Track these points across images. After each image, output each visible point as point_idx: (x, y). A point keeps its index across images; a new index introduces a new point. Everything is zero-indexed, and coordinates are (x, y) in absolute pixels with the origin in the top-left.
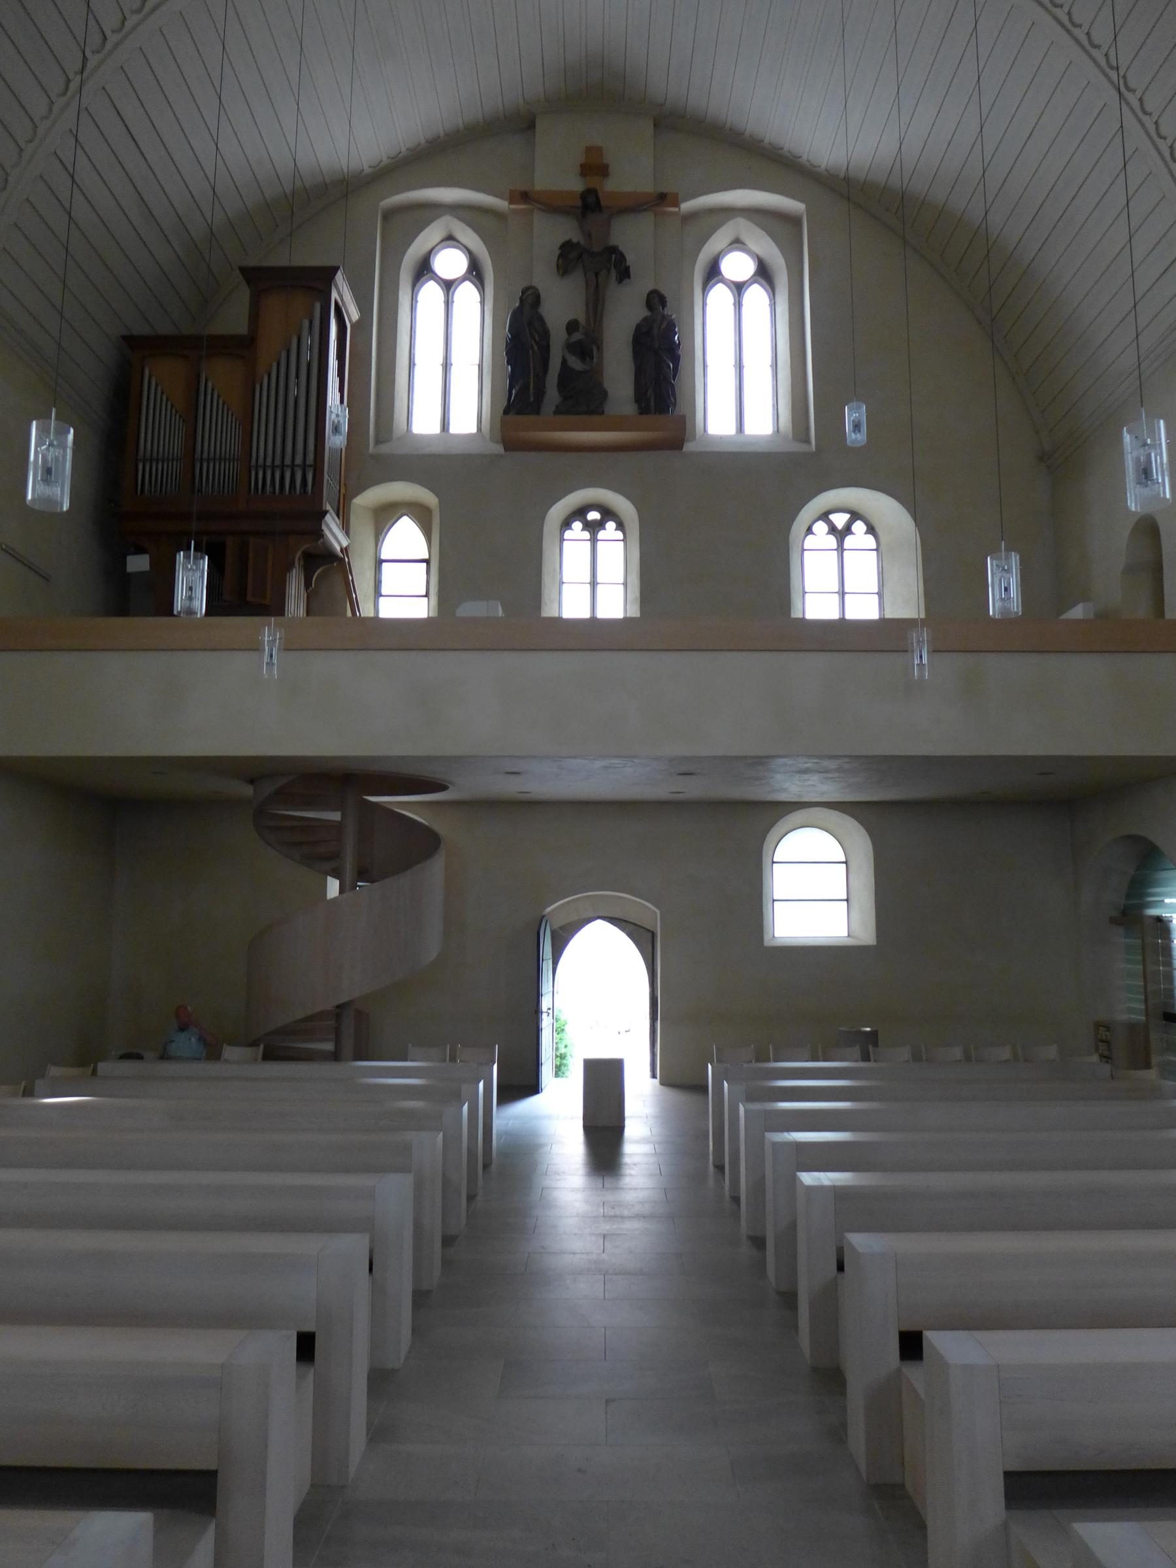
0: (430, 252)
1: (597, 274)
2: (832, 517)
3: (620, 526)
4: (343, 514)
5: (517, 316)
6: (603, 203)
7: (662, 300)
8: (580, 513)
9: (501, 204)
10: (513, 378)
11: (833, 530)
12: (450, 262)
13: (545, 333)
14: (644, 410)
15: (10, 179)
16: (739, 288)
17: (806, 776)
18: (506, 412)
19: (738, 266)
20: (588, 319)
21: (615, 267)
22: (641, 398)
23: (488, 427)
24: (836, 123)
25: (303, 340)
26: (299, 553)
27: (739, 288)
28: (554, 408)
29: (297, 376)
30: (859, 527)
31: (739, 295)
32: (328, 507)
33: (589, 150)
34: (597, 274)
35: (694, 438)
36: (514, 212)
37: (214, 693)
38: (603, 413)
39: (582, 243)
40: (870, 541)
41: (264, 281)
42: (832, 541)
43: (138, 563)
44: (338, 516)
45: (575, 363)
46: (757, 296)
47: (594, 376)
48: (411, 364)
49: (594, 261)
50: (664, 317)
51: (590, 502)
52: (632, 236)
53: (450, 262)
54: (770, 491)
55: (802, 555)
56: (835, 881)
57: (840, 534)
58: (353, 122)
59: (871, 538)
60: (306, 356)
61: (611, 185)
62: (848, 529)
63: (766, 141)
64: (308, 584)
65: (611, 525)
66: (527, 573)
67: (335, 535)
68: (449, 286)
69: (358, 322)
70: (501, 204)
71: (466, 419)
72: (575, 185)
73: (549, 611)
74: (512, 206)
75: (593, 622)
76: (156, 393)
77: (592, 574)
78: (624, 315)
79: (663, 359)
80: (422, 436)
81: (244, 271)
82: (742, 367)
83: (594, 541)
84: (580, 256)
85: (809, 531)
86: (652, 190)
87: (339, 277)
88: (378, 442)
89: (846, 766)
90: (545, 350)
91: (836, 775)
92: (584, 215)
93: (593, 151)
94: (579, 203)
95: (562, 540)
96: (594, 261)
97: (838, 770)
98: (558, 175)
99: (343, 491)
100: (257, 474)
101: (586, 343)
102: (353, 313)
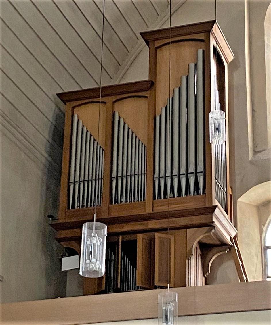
4: (230, 208)
26: (195, 244)
29: (187, 106)
32: (217, 203)
44: (226, 211)
67: (223, 225)
71: (175, 179)
81: (142, 34)
87: (215, 28)
88: (255, 152)
99: (230, 192)
102: (228, 56)
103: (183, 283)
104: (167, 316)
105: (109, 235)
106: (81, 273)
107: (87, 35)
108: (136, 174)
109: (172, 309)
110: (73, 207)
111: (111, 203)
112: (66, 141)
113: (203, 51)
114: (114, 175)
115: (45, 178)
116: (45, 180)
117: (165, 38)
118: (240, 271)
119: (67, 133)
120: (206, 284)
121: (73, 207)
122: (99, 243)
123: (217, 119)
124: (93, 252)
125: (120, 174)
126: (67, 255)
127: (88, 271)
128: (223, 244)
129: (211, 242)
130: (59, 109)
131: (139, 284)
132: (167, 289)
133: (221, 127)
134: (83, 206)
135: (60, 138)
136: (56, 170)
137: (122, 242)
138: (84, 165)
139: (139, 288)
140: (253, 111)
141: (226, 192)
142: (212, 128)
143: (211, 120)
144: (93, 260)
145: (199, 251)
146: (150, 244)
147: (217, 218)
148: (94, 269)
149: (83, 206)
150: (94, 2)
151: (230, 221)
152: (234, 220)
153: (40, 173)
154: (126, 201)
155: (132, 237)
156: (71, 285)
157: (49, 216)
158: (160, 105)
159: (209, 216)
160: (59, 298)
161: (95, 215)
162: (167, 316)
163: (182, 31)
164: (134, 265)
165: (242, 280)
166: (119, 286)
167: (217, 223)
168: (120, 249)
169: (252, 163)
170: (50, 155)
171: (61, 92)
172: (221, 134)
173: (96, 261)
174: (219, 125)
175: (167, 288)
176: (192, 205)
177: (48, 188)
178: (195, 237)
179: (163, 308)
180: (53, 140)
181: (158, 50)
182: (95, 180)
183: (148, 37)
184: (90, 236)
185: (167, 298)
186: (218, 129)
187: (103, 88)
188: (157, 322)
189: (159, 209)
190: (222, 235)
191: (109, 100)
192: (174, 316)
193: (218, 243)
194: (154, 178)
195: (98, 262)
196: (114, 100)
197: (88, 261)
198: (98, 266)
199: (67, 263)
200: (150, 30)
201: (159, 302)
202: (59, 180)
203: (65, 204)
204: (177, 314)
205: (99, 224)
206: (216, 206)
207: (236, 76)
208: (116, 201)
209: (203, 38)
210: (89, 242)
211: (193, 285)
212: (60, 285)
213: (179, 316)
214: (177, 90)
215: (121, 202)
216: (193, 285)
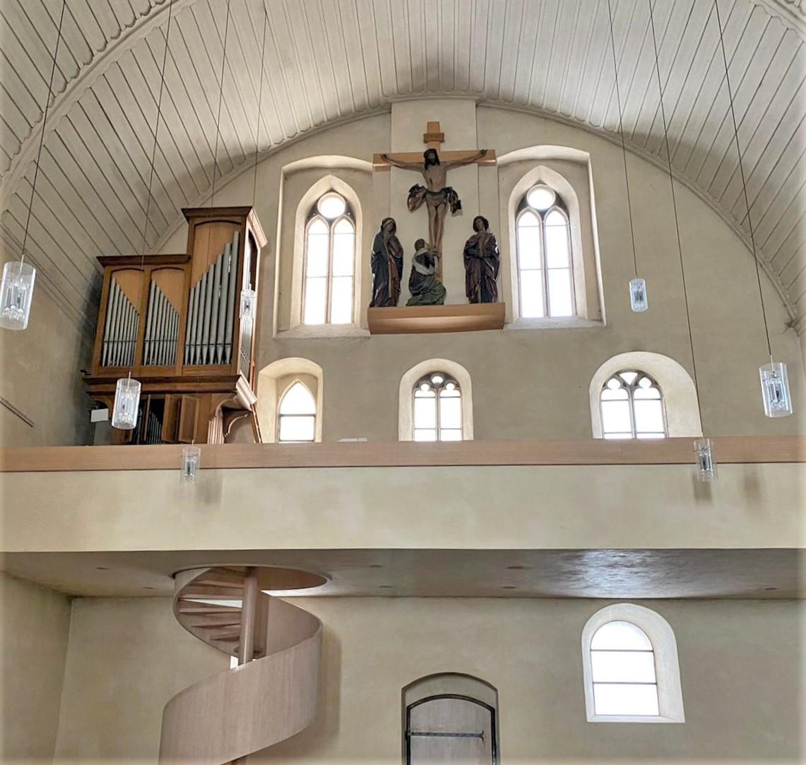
0: (318, 200)
1: (436, 207)
2: (622, 375)
3: (458, 386)
4: (252, 379)
5: (379, 238)
6: (441, 159)
7: (486, 223)
8: (427, 377)
9: (369, 165)
11: (624, 385)
12: (332, 207)
15: (22, 146)
16: (543, 214)
17: (615, 571)
18: (372, 305)
19: (541, 199)
20: (431, 241)
21: (450, 201)
22: (470, 293)
23: (359, 319)
25: (226, 257)
26: (219, 408)
27: (543, 214)
28: (406, 302)
30: (645, 382)
31: (543, 219)
32: (241, 373)
33: (430, 125)
34: (436, 207)
36: (377, 169)
38: (443, 304)
39: (426, 187)
40: (655, 393)
42: (624, 394)
46: (556, 218)
47: (433, 275)
48: (304, 278)
50: (486, 234)
51: (434, 369)
53: (332, 207)
54: (577, 352)
55: (600, 405)
56: (643, 667)
57: (631, 388)
58: (264, 109)
59: (655, 390)
60: (227, 269)
61: (444, 149)
62: (636, 384)
63: (559, 111)
64: (225, 430)
65: (450, 386)
66: (386, 413)
69: (265, 247)
70: (369, 165)
73: (404, 436)
74: (375, 165)
75: (439, 444)
76: (119, 295)
78: (457, 233)
79: (484, 261)
80: (311, 326)
82: (546, 272)
83: (438, 398)
84: (424, 196)
86: (475, 149)
88: (278, 331)
89: (649, 560)
91: (640, 569)
92: (426, 168)
94: (423, 160)
96: (437, 199)
97: (643, 564)
99: (253, 364)
100: (190, 349)
102: (262, 241)
103: (204, 439)
104: (189, 468)
105: (143, 393)
106: (113, 424)
107: (130, 204)
108: (197, 343)
109: (195, 462)
110: (106, 364)
111: (143, 364)
112: (103, 302)
113: (239, 234)
114: (147, 338)
115: (80, 335)
116: (80, 337)
117: (205, 217)
118: (256, 435)
119: (104, 294)
120: (225, 442)
121: (106, 364)
122: (132, 398)
123: (248, 298)
124: (127, 405)
125: (153, 338)
126: (97, 407)
127: (120, 423)
128: (243, 409)
129: (232, 406)
130: (98, 272)
131: (164, 438)
133: (251, 305)
134: (119, 365)
135: (96, 299)
136: (92, 327)
137: (151, 400)
138: (120, 324)
139: (162, 442)
140: (280, 294)
141: (250, 364)
142: (242, 305)
143: (242, 298)
144: (126, 414)
145: (221, 414)
146: (177, 407)
148: (126, 421)
149: (116, 364)
150: (457, 735)
151: (250, 389)
152: (254, 389)
153: (76, 331)
154: (157, 364)
155: (161, 396)
156: (98, 435)
157: (82, 371)
158: (196, 278)
159: (233, 384)
161: (130, 373)
162: (189, 468)
163: (222, 212)
164: (161, 421)
165: (257, 441)
166: (145, 439)
167: (239, 390)
168: (151, 406)
169: (275, 340)
170: (86, 313)
171: (101, 255)
172: (250, 311)
173: (129, 414)
174: (249, 303)
175: (191, 443)
176: (218, 373)
177: (83, 344)
178: (219, 402)
179: (187, 461)
180: (91, 300)
181: (197, 227)
182: (122, 342)
183: (189, 214)
184: (123, 391)
185: (190, 453)
186: (248, 307)
187: (145, 256)
189: (186, 373)
190: (243, 401)
191: (148, 268)
192: (196, 468)
193: (239, 408)
194: (144, 341)
195: (130, 416)
196: (153, 269)
197: (120, 414)
198: (129, 419)
199: (98, 415)
200: (190, 207)
201: (183, 455)
202: (93, 340)
203: (99, 359)
204: (199, 466)
205: (134, 381)
206: (240, 376)
207: (268, 259)
208: (148, 363)
209: (240, 221)
210: (122, 397)
211: (213, 443)
212: (87, 434)
213: (201, 469)
214: (212, 267)
215: (152, 364)
216: (213, 443)
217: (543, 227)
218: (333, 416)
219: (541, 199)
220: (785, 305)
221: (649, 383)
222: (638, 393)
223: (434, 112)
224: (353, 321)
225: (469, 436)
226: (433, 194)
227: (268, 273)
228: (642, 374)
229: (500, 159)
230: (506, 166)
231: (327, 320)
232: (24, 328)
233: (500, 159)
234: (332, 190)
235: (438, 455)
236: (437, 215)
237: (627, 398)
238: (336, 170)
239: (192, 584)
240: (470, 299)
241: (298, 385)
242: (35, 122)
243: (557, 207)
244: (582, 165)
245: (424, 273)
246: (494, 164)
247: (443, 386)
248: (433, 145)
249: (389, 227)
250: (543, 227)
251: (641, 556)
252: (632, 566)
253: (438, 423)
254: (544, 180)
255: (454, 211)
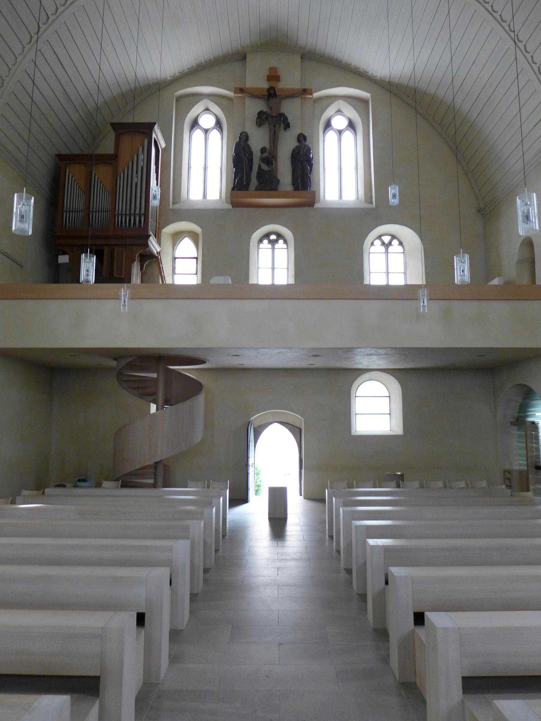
0: (198, 116)
1: (274, 126)
2: (383, 238)
3: (285, 242)
4: (158, 236)
5: (238, 145)
7: (305, 138)
8: (267, 236)
9: (231, 94)
10: (236, 174)
11: (383, 243)
12: (207, 121)
13: (251, 153)
14: (296, 189)
15: (4, 82)
16: (340, 132)
17: (371, 357)
18: (233, 189)
19: (339, 122)
20: (270, 147)
22: (295, 183)
23: (225, 197)
24: (385, 57)
25: (140, 157)
26: (138, 255)
27: (340, 132)
28: (255, 188)
29: (137, 173)
30: (395, 242)
32: (151, 233)
33: (271, 69)
34: (274, 126)
35: (319, 201)
36: (236, 97)
37: (98, 319)
40: (400, 249)
41: (121, 129)
42: (383, 249)
43: (63, 259)
44: (156, 237)
45: (265, 167)
46: (348, 135)
47: (272, 172)
49: (273, 120)
51: (271, 231)
52: (291, 109)
53: (207, 121)
56: (384, 405)
57: (387, 246)
58: (162, 56)
59: (400, 247)
60: (141, 164)
61: (281, 85)
62: (390, 243)
63: (353, 65)
64: (142, 269)
65: (281, 241)
67: (154, 245)
68: (206, 131)
69: (165, 148)
70: (231, 94)
72: (264, 85)
73: (253, 281)
74: (236, 95)
75: (273, 286)
77: (272, 263)
78: (287, 145)
79: (304, 164)
82: (341, 165)
83: (273, 248)
84: (267, 118)
85: (372, 244)
87: (156, 127)
88: (174, 203)
89: (389, 352)
90: (251, 161)
91: (385, 356)
92: (269, 99)
93: (273, 70)
94: (266, 93)
95: (259, 248)
96: (273, 120)
97: (386, 354)
98: (257, 81)
99: (158, 226)
101: (269, 157)
102: (162, 144)
132: (117, 301)
138: (73, 199)
145: (139, 259)
147: (151, 242)
160: (276, 424)
183: (116, 127)
185: (124, 291)
188: (115, 95)
190: (153, 251)
214: (131, 163)
217: (340, 140)
218: (208, 265)
219: (339, 122)
220: (477, 199)
221: (398, 243)
222: (390, 249)
223: (274, 61)
224: (221, 197)
225: (292, 281)
226: (273, 117)
227: (166, 165)
228: (393, 237)
229: (316, 95)
230: (319, 99)
231: (205, 196)
232: (30, 234)
233: (316, 95)
234: (207, 109)
235: (273, 293)
236: (275, 131)
237: (384, 251)
238: (210, 96)
239: (128, 364)
240: (294, 187)
241: (186, 238)
242: (12, 65)
243: (349, 128)
244: (365, 102)
245: (266, 169)
246: (311, 98)
247: (276, 241)
248: (273, 84)
249: (244, 138)
250: (340, 140)
251: (386, 350)
252: (380, 355)
253: (273, 264)
254: (342, 109)
255: (285, 129)
